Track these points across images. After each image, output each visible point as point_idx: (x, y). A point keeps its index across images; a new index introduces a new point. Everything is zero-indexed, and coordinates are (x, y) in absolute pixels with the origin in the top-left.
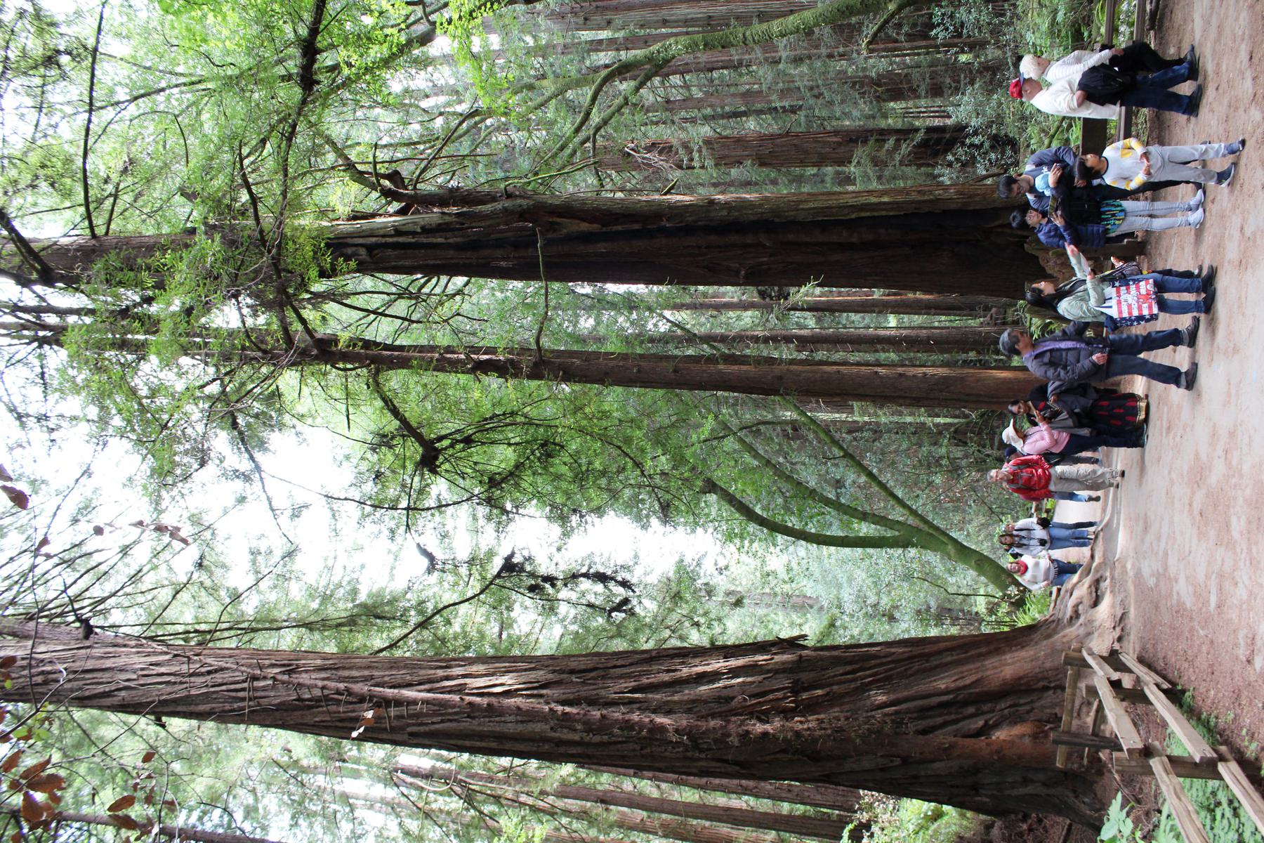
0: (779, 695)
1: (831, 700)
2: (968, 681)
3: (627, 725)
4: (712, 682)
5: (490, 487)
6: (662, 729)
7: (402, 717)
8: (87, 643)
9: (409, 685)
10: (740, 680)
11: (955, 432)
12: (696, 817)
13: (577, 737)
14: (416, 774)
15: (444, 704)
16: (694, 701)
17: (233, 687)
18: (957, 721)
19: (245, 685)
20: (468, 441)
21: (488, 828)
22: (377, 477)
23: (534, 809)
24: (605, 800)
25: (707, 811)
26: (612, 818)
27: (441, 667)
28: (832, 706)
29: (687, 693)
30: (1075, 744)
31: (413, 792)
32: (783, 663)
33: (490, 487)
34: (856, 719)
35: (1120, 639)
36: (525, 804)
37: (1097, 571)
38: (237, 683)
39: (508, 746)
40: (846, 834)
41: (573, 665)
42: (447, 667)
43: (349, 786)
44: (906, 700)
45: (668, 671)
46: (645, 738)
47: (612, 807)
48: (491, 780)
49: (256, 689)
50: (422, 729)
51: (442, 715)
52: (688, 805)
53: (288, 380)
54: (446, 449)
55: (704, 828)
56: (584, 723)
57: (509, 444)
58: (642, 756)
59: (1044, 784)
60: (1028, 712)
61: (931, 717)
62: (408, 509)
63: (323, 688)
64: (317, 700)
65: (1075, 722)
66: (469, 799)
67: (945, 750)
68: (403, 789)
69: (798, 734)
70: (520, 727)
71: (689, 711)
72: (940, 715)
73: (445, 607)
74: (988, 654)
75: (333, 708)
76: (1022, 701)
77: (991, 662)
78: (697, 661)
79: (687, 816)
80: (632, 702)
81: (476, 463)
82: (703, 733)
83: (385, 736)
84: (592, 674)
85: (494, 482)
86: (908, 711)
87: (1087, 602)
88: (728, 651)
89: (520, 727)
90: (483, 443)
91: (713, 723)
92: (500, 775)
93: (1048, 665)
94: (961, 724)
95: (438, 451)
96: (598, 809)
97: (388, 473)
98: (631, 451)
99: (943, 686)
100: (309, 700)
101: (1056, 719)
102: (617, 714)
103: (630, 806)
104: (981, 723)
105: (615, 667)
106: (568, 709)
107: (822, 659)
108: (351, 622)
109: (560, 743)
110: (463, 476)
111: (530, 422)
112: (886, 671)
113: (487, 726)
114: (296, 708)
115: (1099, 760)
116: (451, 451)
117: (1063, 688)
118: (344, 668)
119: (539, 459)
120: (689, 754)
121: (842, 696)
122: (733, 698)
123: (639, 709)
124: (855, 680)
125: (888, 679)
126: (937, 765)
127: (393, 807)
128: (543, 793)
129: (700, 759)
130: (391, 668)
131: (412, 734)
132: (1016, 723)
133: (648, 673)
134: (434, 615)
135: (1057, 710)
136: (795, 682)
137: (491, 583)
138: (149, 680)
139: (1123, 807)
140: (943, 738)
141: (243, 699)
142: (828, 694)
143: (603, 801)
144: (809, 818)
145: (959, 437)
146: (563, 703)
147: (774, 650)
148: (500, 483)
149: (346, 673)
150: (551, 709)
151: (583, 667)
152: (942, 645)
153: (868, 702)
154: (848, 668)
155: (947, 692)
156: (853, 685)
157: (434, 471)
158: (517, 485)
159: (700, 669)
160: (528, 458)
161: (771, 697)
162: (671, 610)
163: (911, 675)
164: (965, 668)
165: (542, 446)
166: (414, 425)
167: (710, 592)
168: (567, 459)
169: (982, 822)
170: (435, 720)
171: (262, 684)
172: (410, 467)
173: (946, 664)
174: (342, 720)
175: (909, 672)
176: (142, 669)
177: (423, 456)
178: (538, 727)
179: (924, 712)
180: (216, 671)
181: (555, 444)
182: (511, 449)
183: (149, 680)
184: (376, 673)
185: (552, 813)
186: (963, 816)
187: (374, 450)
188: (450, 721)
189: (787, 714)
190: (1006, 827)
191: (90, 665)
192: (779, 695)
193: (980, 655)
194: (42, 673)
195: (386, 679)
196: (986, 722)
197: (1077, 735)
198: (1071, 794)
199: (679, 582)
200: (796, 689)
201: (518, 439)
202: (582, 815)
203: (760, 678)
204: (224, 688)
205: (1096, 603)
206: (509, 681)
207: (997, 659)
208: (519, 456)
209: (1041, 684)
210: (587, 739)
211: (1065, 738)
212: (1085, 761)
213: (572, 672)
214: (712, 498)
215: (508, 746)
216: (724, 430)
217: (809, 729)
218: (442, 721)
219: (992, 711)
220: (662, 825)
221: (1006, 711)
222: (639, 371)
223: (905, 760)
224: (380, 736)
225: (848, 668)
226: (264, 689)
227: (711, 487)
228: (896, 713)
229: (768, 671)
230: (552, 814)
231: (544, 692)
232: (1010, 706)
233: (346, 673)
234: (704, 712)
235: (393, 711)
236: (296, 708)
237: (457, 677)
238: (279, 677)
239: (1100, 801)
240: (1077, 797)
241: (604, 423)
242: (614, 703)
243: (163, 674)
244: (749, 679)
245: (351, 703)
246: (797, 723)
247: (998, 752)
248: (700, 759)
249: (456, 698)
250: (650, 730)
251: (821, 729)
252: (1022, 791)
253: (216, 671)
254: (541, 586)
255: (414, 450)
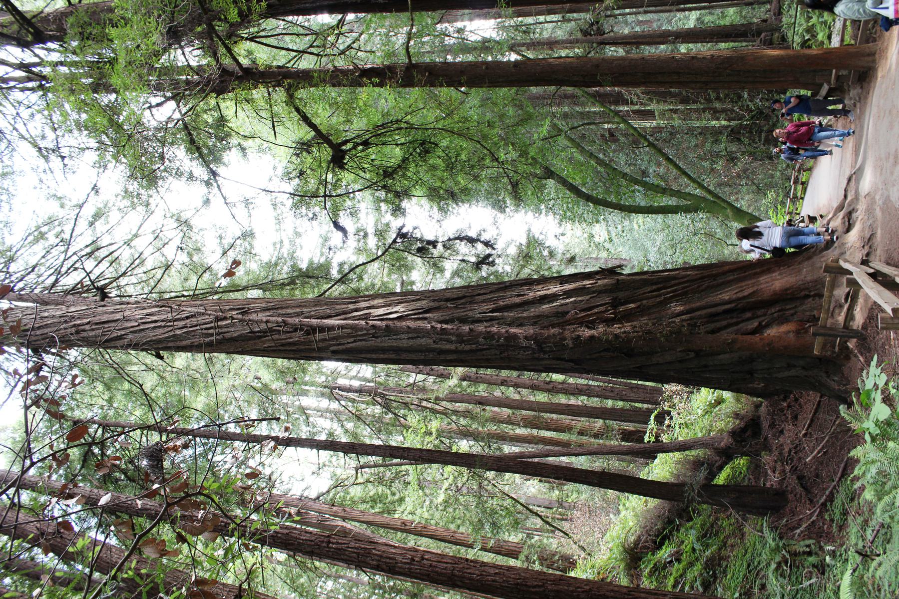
0: (602, 309)
1: (641, 311)
2: (746, 293)
3: (489, 336)
4: (552, 302)
5: (385, 177)
6: (515, 337)
7: (325, 340)
8: (103, 303)
9: (329, 317)
10: (572, 299)
11: (732, 130)
12: (546, 412)
13: (453, 347)
14: (349, 390)
15: (354, 328)
16: (538, 316)
17: (205, 326)
18: (737, 324)
19: (212, 325)
20: (366, 144)
21: (401, 425)
22: (301, 174)
23: (433, 411)
24: (482, 402)
25: (554, 407)
26: (488, 415)
27: (352, 303)
28: (642, 316)
29: (533, 311)
30: (830, 335)
31: (350, 404)
32: (605, 285)
33: (385, 177)
34: (661, 324)
35: (868, 255)
36: (426, 408)
37: (849, 205)
38: (208, 323)
39: (404, 356)
40: (652, 418)
41: (448, 295)
42: (355, 302)
43: (305, 401)
44: (698, 309)
45: (518, 296)
46: (503, 345)
47: (488, 408)
48: (401, 392)
49: (219, 327)
50: (341, 347)
51: (354, 336)
52: (539, 403)
53: (228, 106)
54: (350, 150)
55: (552, 420)
56: (457, 336)
57: (397, 145)
58: (502, 358)
59: (803, 368)
60: (792, 315)
61: (717, 321)
62: (325, 196)
63: (267, 322)
64: (265, 332)
65: (830, 321)
66: (387, 407)
67: (729, 344)
68: (343, 403)
69: (617, 336)
70: (411, 342)
71: (535, 324)
72: (725, 319)
73: (357, 267)
74: (762, 273)
75: (276, 337)
76: (788, 307)
77: (763, 279)
78: (540, 287)
79: (540, 411)
80: (492, 319)
81: (372, 160)
82: (546, 338)
83: (314, 355)
84: (462, 301)
85: (388, 173)
86: (700, 317)
87: (840, 229)
88: (563, 279)
89: (411, 342)
90: (377, 145)
91: (552, 331)
92: (408, 389)
93: (809, 278)
94: (741, 325)
95: (344, 153)
96: (477, 409)
97: (309, 171)
98: (488, 145)
99: (727, 298)
100: (258, 332)
101: (815, 319)
102: (481, 328)
103: (499, 406)
104: (756, 324)
105: (479, 295)
106: (445, 326)
107: (634, 281)
108: (292, 282)
109: (441, 352)
110: (364, 170)
111: (411, 127)
112: (683, 288)
113: (387, 342)
114: (251, 339)
115: (848, 347)
116: (354, 152)
117: (821, 296)
118: (282, 308)
119: (420, 154)
120: (536, 355)
121: (649, 308)
122: (568, 313)
123: (498, 323)
124: (660, 296)
125: (685, 294)
126: (722, 356)
127: (336, 414)
128: (437, 398)
129: (543, 359)
130: (316, 305)
131: (333, 352)
132: (783, 323)
133: (503, 297)
134: (349, 273)
135: (815, 312)
136: (614, 299)
137: (389, 247)
138: (147, 326)
139: (877, 367)
140: (727, 336)
141: (212, 335)
142: (639, 307)
143: (480, 403)
144: (627, 410)
145: (734, 135)
146: (441, 322)
147: (598, 277)
148: (392, 174)
149: (284, 311)
150: (432, 327)
151: (455, 296)
152: (726, 268)
153: (669, 312)
154: (654, 287)
155: (730, 302)
156: (658, 299)
157: (342, 167)
158: (404, 176)
159: (542, 293)
160: (411, 154)
161: (596, 310)
162: (523, 267)
163: (702, 291)
164: (743, 284)
165: (422, 144)
166: (324, 132)
167: (552, 254)
168: (441, 154)
169: (753, 403)
170: (349, 341)
171: (225, 323)
172: (324, 165)
173: (729, 282)
174: (283, 345)
175: (701, 288)
176: (141, 319)
177: (333, 156)
178: (423, 341)
179: (712, 317)
180: (192, 316)
181: (430, 142)
182: (398, 149)
183: (147, 326)
184: (305, 310)
185: (445, 413)
186: (738, 401)
187: (297, 155)
188: (361, 340)
189: (609, 322)
190: (771, 405)
191: (105, 318)
192: (602, 309)
193: (755, 274)
194: (74, 326)
195: (313, 313)
196: (760, 324)
197: (831, 329)
198: (824, 375)
199: (528, 247)
200: (615, 304)
201: (403, 140)
202: (467, 414)
203: (587, 297)
204: (198, 328)
205: (848, 230)
206: (401, 309)
207: (769, 275)
208: (405, 153)
209: (803, 293)
210: (460, 348)
211: (822, 331)
212: (837, 349)
213: (447, 300)
214: (551, 183)
215: (404, 356)
216: (557, 130)
217: (625, 332)
218: (355, 341)
219: (765, 315)
220: (523, 419)
221: (775, 315)
222: (487, 68)
223: (698, 353)
224: (311, 355)
225: (654, 287)
226: (226, 326)
227: (549, 174)
228: (691, 319)
229: (594, 292)
230: (446, 414)
231: (427, 315)
232: (779, 311)
233: (284, 311)
234: (546, 324)
235: (318, 336)
236: (251, 339)
237: (364, 308)
238: (235, 316)
239: (847, 378)
240: (828, 377)
241: (466, 125)
242: (479, 321)
243: (156, 321)
244: (580, 299)
245: (289, 332)
246: (616, 329)
247: (769, 345)
248: (543, 359)
249: (363, 323)
250: (506, 338)
251: (634, 332)
252: (786, 374)
253: (192, 316)
254: (425, 248)
255: (326, 153)
